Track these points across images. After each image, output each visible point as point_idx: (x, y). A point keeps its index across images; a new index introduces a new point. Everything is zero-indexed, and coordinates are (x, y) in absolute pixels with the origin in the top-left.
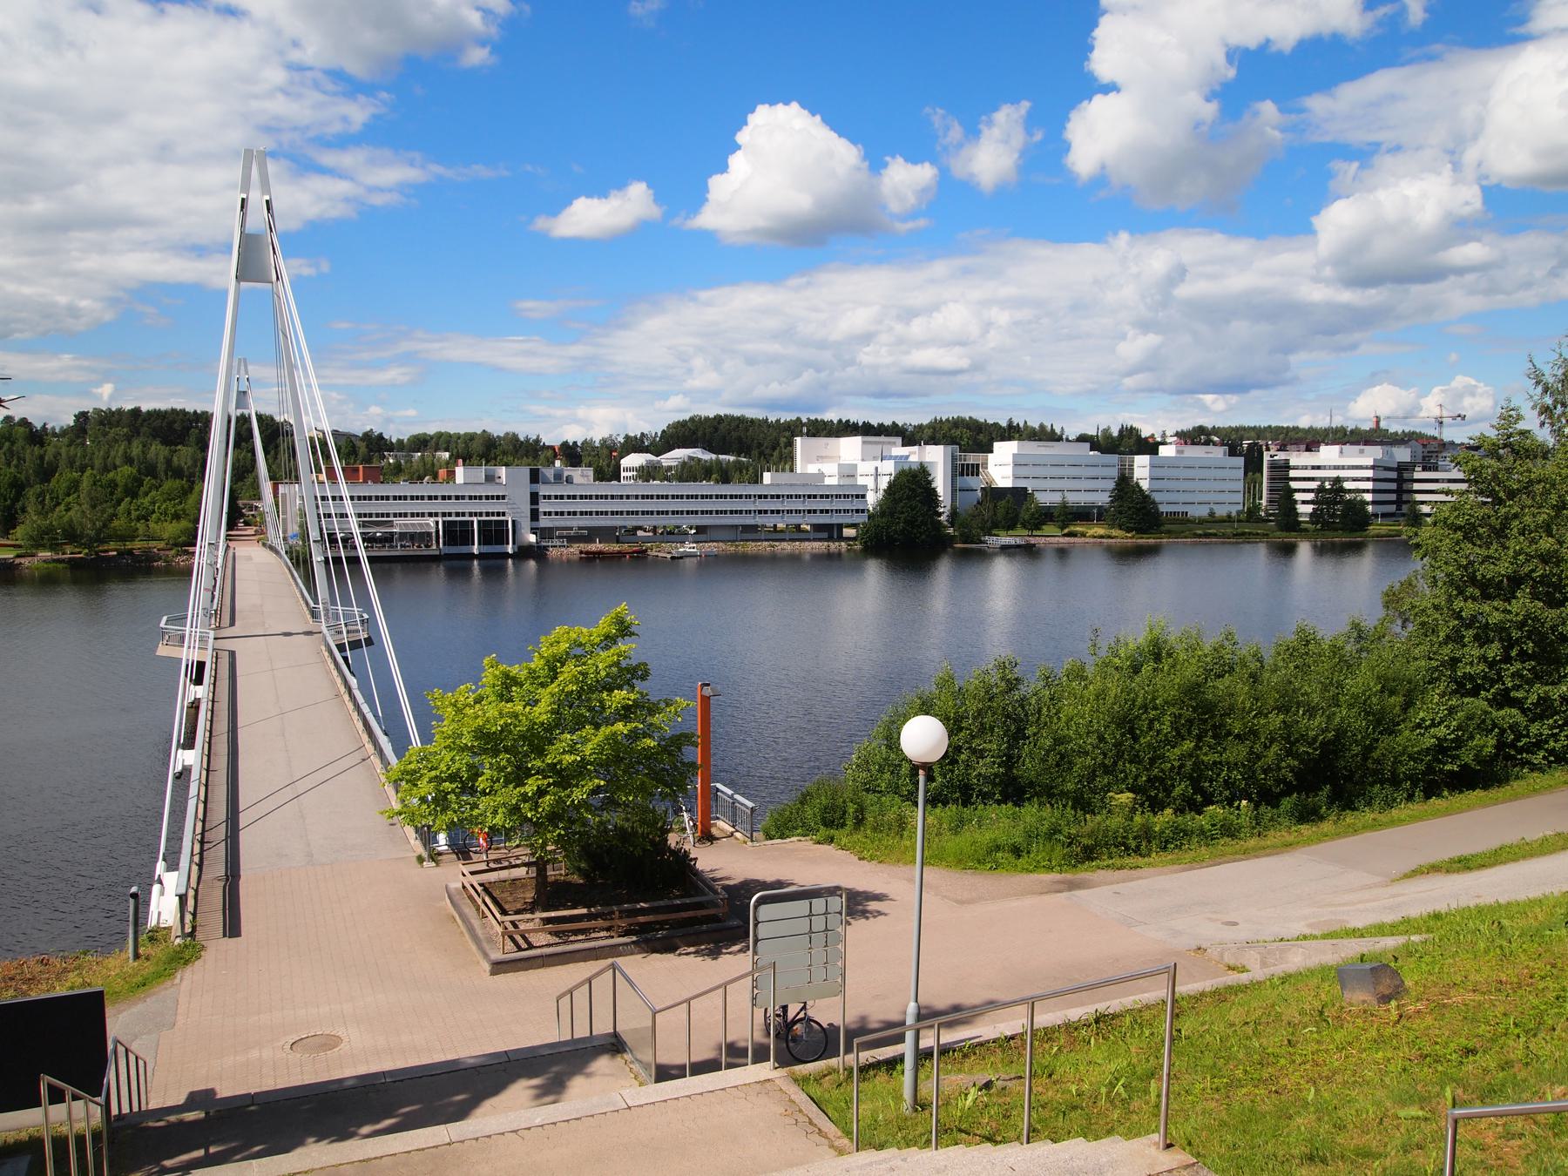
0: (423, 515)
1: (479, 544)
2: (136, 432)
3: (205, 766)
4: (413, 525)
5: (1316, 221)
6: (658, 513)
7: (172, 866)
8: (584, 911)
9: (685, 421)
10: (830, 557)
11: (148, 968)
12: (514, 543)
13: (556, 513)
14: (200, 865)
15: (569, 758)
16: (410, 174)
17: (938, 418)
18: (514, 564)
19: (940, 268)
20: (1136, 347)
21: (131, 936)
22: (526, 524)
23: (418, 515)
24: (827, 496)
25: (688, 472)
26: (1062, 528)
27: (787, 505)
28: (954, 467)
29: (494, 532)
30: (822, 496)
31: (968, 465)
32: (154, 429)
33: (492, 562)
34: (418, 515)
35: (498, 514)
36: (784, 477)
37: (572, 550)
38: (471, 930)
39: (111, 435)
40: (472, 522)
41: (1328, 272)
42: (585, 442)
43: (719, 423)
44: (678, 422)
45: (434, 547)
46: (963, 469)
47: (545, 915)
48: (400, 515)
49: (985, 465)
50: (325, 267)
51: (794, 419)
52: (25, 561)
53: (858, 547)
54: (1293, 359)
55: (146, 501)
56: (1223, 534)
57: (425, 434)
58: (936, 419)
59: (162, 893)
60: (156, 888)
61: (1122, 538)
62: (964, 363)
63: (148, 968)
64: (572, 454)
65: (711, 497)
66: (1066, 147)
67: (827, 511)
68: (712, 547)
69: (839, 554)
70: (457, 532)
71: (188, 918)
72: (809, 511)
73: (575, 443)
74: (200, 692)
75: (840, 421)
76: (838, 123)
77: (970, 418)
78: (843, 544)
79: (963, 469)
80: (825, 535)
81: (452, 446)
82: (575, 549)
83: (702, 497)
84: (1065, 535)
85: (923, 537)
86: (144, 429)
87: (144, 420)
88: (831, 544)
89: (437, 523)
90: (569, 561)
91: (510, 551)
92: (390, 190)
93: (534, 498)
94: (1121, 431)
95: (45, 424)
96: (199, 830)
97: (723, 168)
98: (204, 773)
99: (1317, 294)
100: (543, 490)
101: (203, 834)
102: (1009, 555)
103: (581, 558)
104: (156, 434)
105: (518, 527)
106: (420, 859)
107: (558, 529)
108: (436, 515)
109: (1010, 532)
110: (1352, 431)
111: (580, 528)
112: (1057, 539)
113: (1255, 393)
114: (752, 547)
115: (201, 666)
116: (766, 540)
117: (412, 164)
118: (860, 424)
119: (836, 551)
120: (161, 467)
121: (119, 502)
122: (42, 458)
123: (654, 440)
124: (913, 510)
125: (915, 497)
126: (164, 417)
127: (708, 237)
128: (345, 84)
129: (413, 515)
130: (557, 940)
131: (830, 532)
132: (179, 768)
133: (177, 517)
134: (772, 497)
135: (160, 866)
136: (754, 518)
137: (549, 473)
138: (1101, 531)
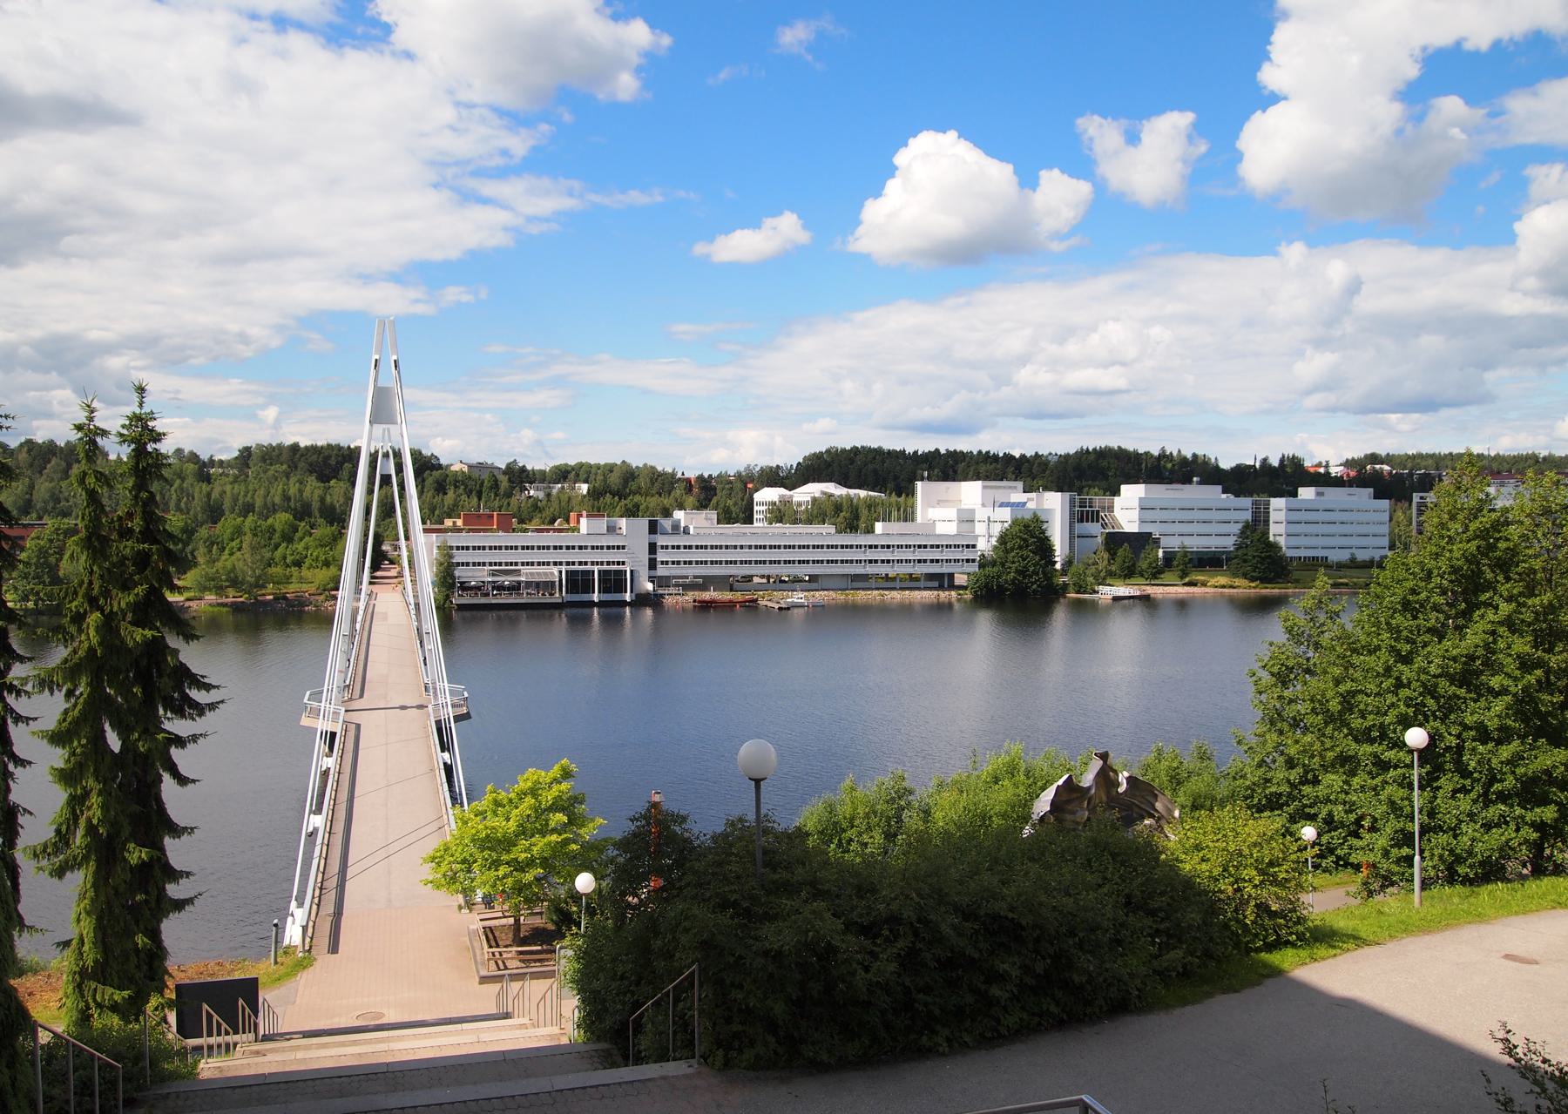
0: (548, 564)
1: (599, 592)
2: (293, 466)
3: (328, 829)
4: (538, 574)
5: (1518, 227)
6: (771, 562)
7: (301, 905)
8: (539, 948)
9: (821, 453)
10: (942, 608)
11: (283, 970)
12: (632, 592)
13: (673, 563)
14: (318, 905)
15: (523, 856)
16: (568, 203)
17: (1085, 448)
18: (631, 612)
19: (1104, 283)
20: (1315, 365)
21: (273, 953)
22: (644, 573)
23: (544, 564)
24: (938, 546)
25: (820, 512)
26: (1182, 578)
27: (897, 555)
28: (1072, 514)
29: (613, 581)
30: (932, 546)
31: (1093, 511)
32: (311, 465)
33: (608, 610)
34: (544, 564)
35: (618, 563)
36: (896, 527)
37: (687, 598)
38: (475, 956)
39: (270, 473)
40: (593, 571)
41: (1531, 283)
42: (720, 476)
43: (856, 454)
44: (814, 454)
45: (557, 595)
46: (1082, 515)
47: (520, 949)
48: (528, 564)
49: (1111, 508)
50: (483, 295)
51: (933, 450)
52: (192, 604)
53: (968, 596)
54: (1490, 376)
55: (300, 546)
56: (1355, 584)
57: (566, 465)
58: (1082, 449)
59: (294, 923)
60: (290, 919)
61: (1246, 588)
62: (1121, 383)
63: (283, 970)
64: (705, 492)
65: (822, 547)
66: (1239, 157)
67: (937, 561)
68: (820, 596)
69: (950, 606)
70: (578, 581)
71: (308, 940)
72: (919, 561)
73: (710, 476)
74: (330, 762)
75: (980, 452)
76: (992, 149)
77: (1119, 447)
78: (953, 593)
79: (1082, 515)
80: (936, 584)
81: (592, 477)
82: (690, 596)
83: (814, 547)
84: (1184, 585)
85: (1035, 586)
86: (302, 464)
87: (302, 455)
88: (941, 593)
89: (560, 572)
90: (684, 609)
91: (628, 599)
92: (547, 220)
93: (653, 548)
94: (1282, 460)
95: (212, 456)
96: (319, 880)
97: (878, 192)
98: (327, 835)
99: (1513, 305)
100: (661, 540)
101: (322, 883)
102: (1126, 609)
103: (695, 606)
104: (311, 469)
105: (636, 575)
106: (460, 908)
107: (674, 577)
108: (561, 563)
109: (1127, 581)
110: (1545, 459)
111: (695, 577)
112: (1175, 588)
113: (1445, 413)
114: (862, 596)
115: (333, 735)
116: (877, 589)
117: (570, 194)
118: (1001, 455)
119: (947, 600)
120: (316, 505)
121: (277, 547)
122: (209, 495)
123: (790, 472)
124: (1024, 560)
125: (1027, 546)
126: (320, 453)
127: (865, 259)
128: (514, 119)
129: (539, 564)
130: (523, 965)
131: (943, 581)
132: (311, 829)
133: (327, 564)
134: (883, 547)
135: (293, 904)
136: (865, 567)
137: (666, 523)
138: (1222, 580)
